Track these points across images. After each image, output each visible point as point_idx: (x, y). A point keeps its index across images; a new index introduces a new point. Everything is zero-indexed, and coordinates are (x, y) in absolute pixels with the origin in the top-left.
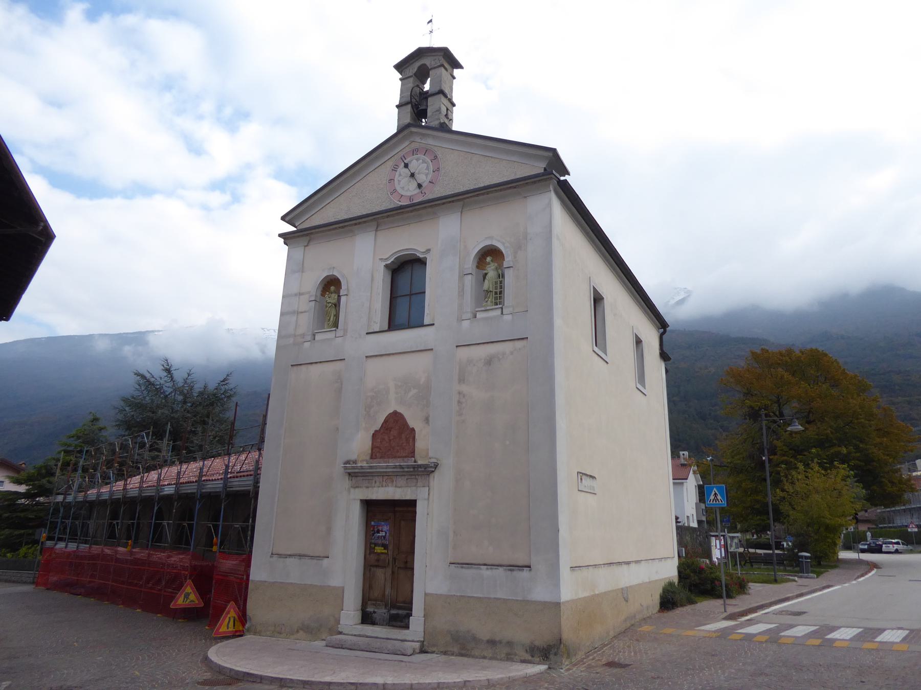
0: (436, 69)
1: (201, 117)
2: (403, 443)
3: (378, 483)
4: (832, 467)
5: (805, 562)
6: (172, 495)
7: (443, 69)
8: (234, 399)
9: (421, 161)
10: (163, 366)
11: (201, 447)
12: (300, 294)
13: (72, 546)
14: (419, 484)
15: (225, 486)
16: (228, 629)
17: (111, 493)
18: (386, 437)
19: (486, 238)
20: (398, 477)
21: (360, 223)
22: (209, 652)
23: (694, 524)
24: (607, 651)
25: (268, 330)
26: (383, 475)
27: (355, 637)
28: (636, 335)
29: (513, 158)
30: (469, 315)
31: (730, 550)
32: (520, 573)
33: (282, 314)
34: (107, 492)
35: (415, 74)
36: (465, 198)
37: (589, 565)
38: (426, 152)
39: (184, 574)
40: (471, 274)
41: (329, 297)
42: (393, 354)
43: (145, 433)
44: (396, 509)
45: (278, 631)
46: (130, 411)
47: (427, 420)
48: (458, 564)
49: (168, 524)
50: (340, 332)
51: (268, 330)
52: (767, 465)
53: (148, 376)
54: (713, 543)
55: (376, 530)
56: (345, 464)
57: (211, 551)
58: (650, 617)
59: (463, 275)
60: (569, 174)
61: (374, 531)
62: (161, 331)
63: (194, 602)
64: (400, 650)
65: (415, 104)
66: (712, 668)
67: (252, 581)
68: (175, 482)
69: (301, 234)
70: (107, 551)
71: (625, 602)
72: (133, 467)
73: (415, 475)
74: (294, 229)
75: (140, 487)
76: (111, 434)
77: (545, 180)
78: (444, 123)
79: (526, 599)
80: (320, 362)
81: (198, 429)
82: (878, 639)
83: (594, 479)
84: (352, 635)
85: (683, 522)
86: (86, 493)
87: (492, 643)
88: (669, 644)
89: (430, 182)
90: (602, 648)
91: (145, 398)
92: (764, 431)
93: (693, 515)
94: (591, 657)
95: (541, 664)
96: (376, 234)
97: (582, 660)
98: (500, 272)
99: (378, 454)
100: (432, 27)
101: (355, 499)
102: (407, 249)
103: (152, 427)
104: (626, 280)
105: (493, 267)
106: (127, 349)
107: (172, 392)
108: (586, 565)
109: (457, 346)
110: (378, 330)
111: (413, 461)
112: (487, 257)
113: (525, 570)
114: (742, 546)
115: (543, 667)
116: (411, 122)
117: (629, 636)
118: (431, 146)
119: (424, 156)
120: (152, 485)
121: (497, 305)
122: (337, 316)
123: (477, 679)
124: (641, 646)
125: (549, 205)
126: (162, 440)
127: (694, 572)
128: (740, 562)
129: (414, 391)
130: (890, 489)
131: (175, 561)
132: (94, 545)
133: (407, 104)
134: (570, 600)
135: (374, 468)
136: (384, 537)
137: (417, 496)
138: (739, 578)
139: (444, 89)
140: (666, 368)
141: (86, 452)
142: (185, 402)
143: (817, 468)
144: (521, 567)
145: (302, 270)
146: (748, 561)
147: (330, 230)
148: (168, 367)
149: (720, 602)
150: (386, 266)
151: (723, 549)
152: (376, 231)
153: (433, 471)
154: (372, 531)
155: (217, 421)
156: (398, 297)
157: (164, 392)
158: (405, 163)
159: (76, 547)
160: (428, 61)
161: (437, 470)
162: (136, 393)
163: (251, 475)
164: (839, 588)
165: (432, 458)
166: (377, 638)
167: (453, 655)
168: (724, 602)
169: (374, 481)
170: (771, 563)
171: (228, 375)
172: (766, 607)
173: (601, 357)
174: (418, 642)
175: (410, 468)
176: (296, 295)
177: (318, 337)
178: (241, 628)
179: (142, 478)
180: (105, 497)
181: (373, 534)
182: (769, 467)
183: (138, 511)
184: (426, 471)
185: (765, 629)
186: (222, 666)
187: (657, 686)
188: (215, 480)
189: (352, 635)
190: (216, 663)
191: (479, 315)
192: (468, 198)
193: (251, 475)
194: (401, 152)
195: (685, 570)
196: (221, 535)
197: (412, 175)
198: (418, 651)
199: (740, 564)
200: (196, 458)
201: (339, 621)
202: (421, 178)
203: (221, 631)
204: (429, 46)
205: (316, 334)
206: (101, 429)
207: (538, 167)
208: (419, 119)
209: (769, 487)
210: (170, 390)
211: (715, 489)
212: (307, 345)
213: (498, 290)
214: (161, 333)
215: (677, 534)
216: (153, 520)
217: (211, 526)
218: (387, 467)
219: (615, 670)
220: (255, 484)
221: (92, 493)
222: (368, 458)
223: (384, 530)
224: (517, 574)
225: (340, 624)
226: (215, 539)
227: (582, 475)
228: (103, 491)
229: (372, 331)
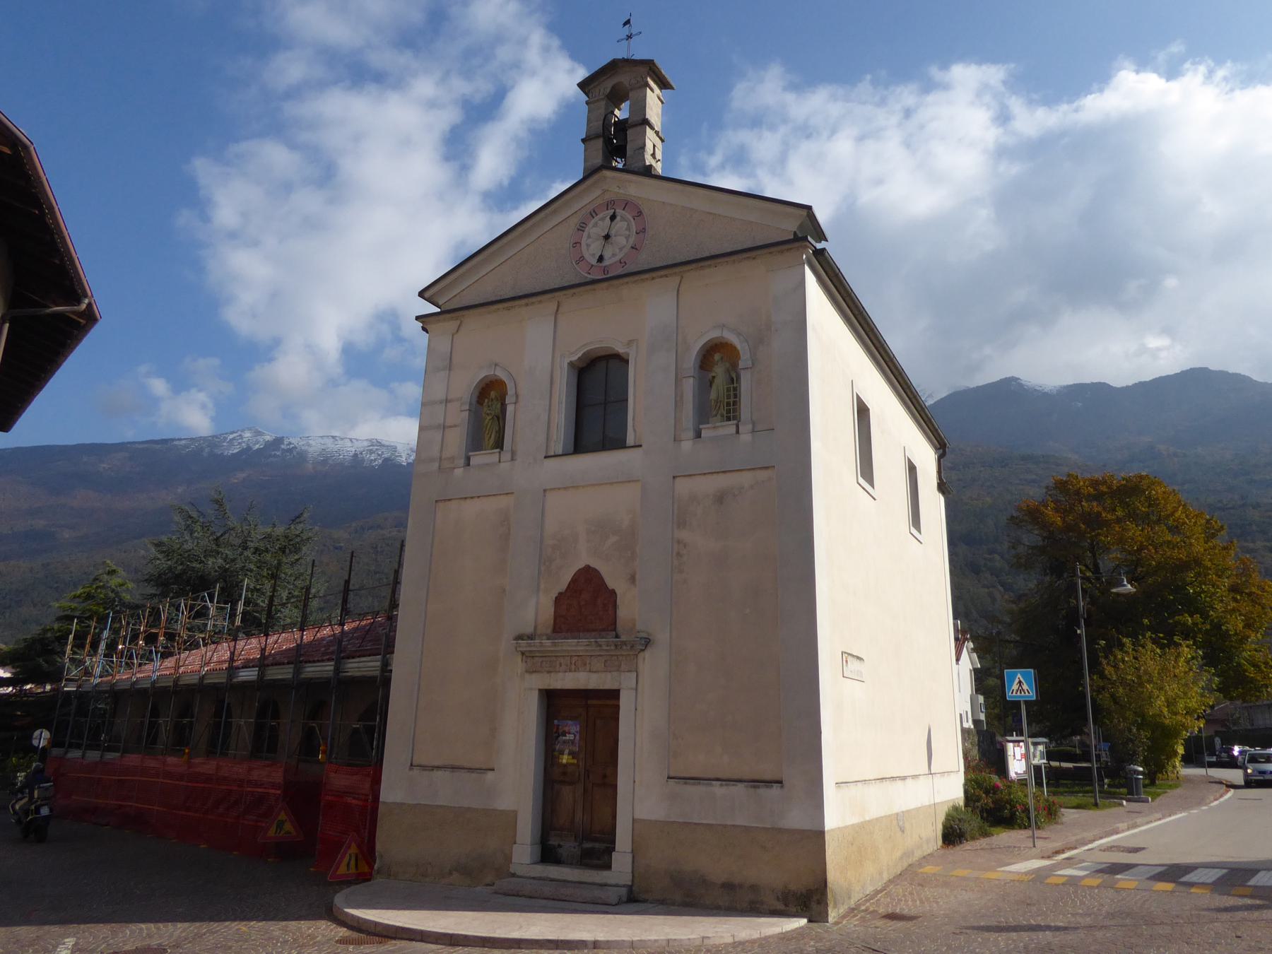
4: (1172, 644)
6: (194, 685)
13: (93, 756)
22: (336, 897)
50: (506, 456)
58: (931, 855)
63: (290, 833)
67: (384, 803)
80: (494, 495)
82: (1252, 882)
88: (966, 890)
89: (632, 248)
93: (967, 712)
101: (531, 689)
112: (715, 353)
113: (775, 787)
117: (908, 879)
119: (623, 212)
127: (987, 792)
129: (613, 539)
133: (597, 137)
143: (1150, 645)
144: (769, 783)
149: (1028, 833)
154: (556, 732)
159: (99, 756)
164: (1184, 817)
178: (366, 869)
186: (362, 919)
196: (1085, 706)
197: (607, 237)
198: (624, 899)
203: (339, 872)
207: (789, 226)
211: (1019, 675)
213: (732, 400)
222: (549, 631)
223: (572, 731)
224: (763, 792)
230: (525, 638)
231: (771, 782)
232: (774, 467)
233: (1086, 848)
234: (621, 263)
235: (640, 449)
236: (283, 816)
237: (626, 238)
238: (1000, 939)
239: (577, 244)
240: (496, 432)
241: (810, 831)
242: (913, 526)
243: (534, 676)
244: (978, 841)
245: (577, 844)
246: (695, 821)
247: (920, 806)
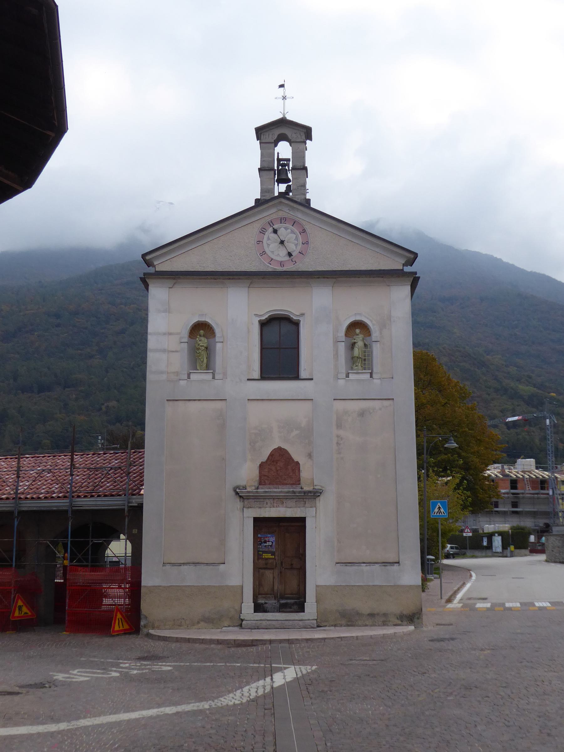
0: (298, 144)
2: (290, 473)
3: (269, 504)
5: (431, 564)
9: (289, 230)
14: (307, 505)
26: (273, 498)
29: (377, 250)
32: (392, 567)
41: (200, 341)
44: (281, 524)
47: (310, 456)
48: (342, 563)
59: (336, 342)
61: (261, 541)
64: (309, 625)
73: (303, 499)
84: (254, 620)
87: (372, 615)
99: (266, 481)
100: (284, 93)
115: (412, 628)
119: (292, 227)
121: (366, 370)
129: (295, 432)
130: (481, 496)
136: (271, 546)
137: (306, 514)
144: (392, 563)
150: (260, 321)
153: (319, 496)
158: (273, 228)
175: (301, 493)
176: (164, 334)
177: (192, 376)
181: (260, 544)
184: (315, 494)
197: (282, 242)
202: (291, 247)
211: (439, 504)
218: (281, 492)
224: (389, 568)
234: (292, 261)
235: (312, 381)
239: (259, 242)
240: (207, 358)
241: (414, 585)
245: (277, 601)
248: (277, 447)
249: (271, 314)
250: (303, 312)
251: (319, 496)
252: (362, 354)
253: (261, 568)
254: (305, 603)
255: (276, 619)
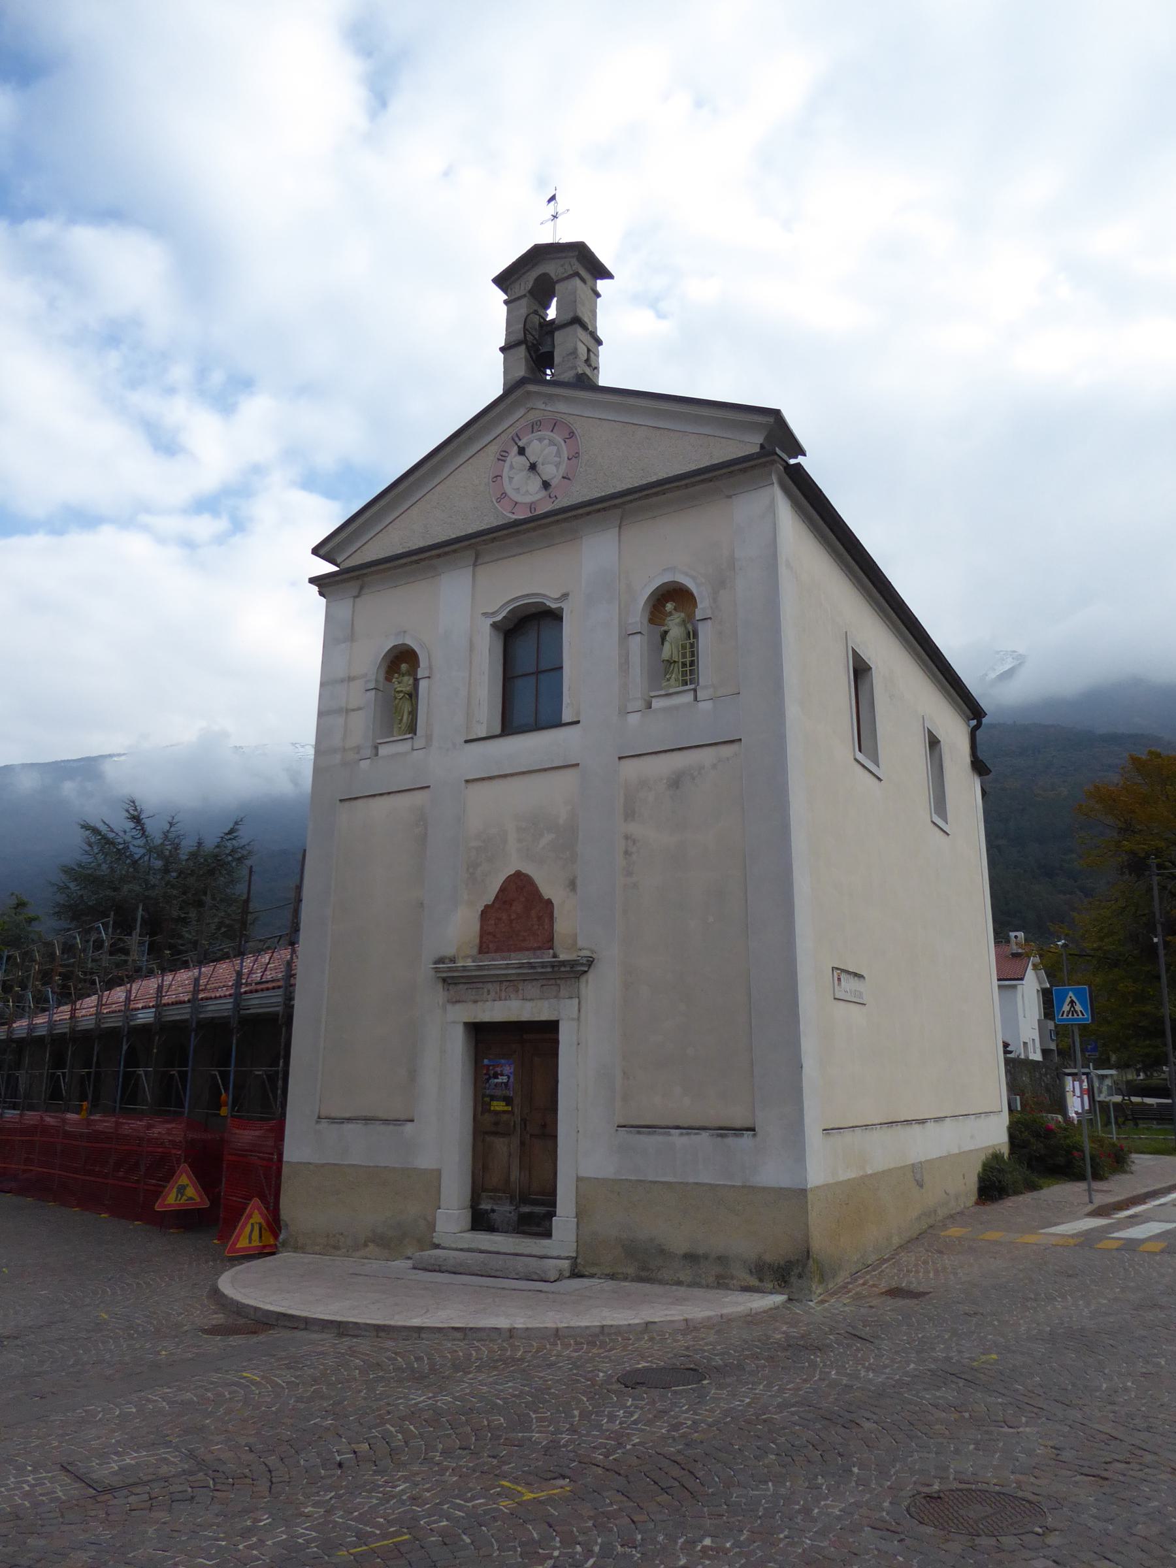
1: (171, 391)
3: (493, 994)
6: (91, 1030)
7: (578, 281)
8: (248, 862)
9: (546, 442)
10: (127, 811)
11: (195, 944)
12: (351, 679)
14: (563, 993)
15: (237, 1005)
16: (250, 1243)
17: (52, 1024)
18: (505, 917)
19: (664, 570)
20: (526, 983)
21: (446, 554)
22: (220, 1280)
23: (1037, 1056)
24: (888, 1270)
25: (303, 746)
26: (501, 980)
27: (462, 1253)
28: (929, 731)
29: (707, 430)
30: (639, 704)
31: (1098, 1099)
33: (321, 714)
34: (44, 1023)
35: (531, 292)
36: (624, 503)
37: (854, 1125)
38: (554, 426)
39: (175, 1154)
40: (640, 633)
41: (399, 683)
42: (512, 775)
43: (102, 923)
45: (332, 1245)
46: (78, 888)
47: (572, 885)
48: (632, 1127)
49: (146, 1073)
50: (419, 742)
51: (303, 746)
52: (1161, 952)
53: (103, 829)
54: (1069, 1087)
55: (492, 1072)
56: (435, 963)
57: (219, 1114)
58: (961, 1213)
60: (804, 454)
61: (489, 1075)
62: (124, 754)
63: (194, 1199)
65: (533, 343)
66: (1069, 1297)
68: (154, 1003)
69: (346, 576)
70: (49, 1120)
71: (918, 1187)
72: (85, 981)
74: (334, 568)
75: (98, 1013)
76: (48, 927)
77: (764, 465)
78: (584, 374)
79: (748, 1184)
81: (190, 915)
83: (862, 979)
84: (457, 1249)
85: (1017, 1053)
86: (10, 1027)
87: (691, 1258)
88: (995, 1258)
90: (879, 1266)
91: (99, 865)
92: (1156, 892)
94: (861, 1281)
95: (775, 1293)
96: (474, 570)
97: (844, 1287)
98: (690, 628)
99: (491, 946)
102: (528, 595)
103: (112, 913)
104: (910, 635)
105: (678, 620)
106: (69, 788)
107: (144, 855)
108: (851, 1125)
109: (620, 758)
110: (484, 735)
111: (551, 956)
113: (746, 1136)
114: (1119, 1091)
115: (779, 1299)
116: (527, 375)
118: (563, 416)
119: (552, 434)
120: (117, 1009)
122: (414, 714)
123: (669, 1318)
124: (947, 1261)
125: (772, 508)
126: (130, 934)
128: (1116, 1118)
129: (548, 838)
131: (159, 1133)
132: (27, 1110)
134: (823, 1186)
135: (485, 969)
136: (506, 1084)
138: (1114, 1145)
139: (580, 314)
140: (982, 787)
141: (7, 959)
142: (166, 870)
144: (738, 1131)
145: (352, 637)
146: (1128, 1116)
147: (395, 568)
148: (136, 813)
150: (495, 626)
151: (1086, 1097)
152: (475, 565)
153: (586, 972)
154: (485, 1074)
155: (222, 900)
156: (513, 678)
157: (131, 855)
158: (519, 447)
160: (551, 268)
161: (591, 970)
162: (86, 859)
163: (279, 987)
165: (584, 949)
166: (498, 1253)
167: (625, 1279)
168: (1089, 1186)
169: (486, 990)
170: (1169, 1119)
171: (236, 823)
172: (1163, 1193)
173: (871, 772)
174: (567, 1258)
175: (546, 967)
176: (342, 681)
177: (383, 751)
178: (272, 1242)
179: (100, 999)
180: (42, 1032)
181: (488, 1080)
182: (1166, 955)
183: (95, 1053)
185: (1159, 1231)
187: (973, 1328)
188: (220, 997)
189: (457, 1249)
190: (232, 1299)
191: (656, 704)
192: (631, 501)
193: (279, 987)
194: (518, 423)
195: (1021, 1132)
197: (533, 467)
198: (568, 1274)
199: (1116, 1123)
200: (186, 962)
201: (435, 1226)
202: (549, 471)
203: (239, 1246)
204: (552, 242)
205: (380, 747)
206: (30, 921)
207: (750, 443)
208: (540, 370)
209: (1165, 991)
210: (142, 851)
211: (1071, 994)
212: (364, 765)
213: (688, 660)
214: (123, 758)
215: (1007, 1072)
216: (122, 1067)
217: (217, 1073)
218: (508, 966)
219: (900, 1302)
220: (287, 1002)
221: (20, 1026)
222: (475, 951)
223: (505, 1072)
224: (731, 1141)
225: (435, 1232)
226: (224, 1094)
227: (840, 972)
228: (38, 1022)
229: (475, 737)
230: (447, 961)
231: (741, 1130)
232: (740, 740)
233: (1157, 1202)
234: (550, 497)
236: (184, 1180)
237: (556, 466)
238: (1021, 1321)
242: (935, 813)
243: (458, 1007)
244: (1023, 1195)
246: (650, 1179)
247: (945, 1154)
248: (512, 872)
249: (508, 609)
250: (564, 591)
251: (586, 972)
252: (679, 651)
253: (486, 1133)
254: (554, 1218)
255: (496, 1250)
